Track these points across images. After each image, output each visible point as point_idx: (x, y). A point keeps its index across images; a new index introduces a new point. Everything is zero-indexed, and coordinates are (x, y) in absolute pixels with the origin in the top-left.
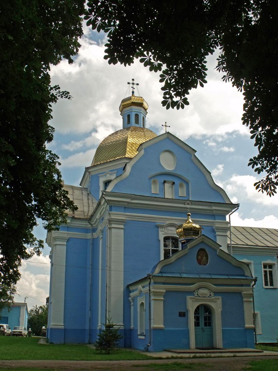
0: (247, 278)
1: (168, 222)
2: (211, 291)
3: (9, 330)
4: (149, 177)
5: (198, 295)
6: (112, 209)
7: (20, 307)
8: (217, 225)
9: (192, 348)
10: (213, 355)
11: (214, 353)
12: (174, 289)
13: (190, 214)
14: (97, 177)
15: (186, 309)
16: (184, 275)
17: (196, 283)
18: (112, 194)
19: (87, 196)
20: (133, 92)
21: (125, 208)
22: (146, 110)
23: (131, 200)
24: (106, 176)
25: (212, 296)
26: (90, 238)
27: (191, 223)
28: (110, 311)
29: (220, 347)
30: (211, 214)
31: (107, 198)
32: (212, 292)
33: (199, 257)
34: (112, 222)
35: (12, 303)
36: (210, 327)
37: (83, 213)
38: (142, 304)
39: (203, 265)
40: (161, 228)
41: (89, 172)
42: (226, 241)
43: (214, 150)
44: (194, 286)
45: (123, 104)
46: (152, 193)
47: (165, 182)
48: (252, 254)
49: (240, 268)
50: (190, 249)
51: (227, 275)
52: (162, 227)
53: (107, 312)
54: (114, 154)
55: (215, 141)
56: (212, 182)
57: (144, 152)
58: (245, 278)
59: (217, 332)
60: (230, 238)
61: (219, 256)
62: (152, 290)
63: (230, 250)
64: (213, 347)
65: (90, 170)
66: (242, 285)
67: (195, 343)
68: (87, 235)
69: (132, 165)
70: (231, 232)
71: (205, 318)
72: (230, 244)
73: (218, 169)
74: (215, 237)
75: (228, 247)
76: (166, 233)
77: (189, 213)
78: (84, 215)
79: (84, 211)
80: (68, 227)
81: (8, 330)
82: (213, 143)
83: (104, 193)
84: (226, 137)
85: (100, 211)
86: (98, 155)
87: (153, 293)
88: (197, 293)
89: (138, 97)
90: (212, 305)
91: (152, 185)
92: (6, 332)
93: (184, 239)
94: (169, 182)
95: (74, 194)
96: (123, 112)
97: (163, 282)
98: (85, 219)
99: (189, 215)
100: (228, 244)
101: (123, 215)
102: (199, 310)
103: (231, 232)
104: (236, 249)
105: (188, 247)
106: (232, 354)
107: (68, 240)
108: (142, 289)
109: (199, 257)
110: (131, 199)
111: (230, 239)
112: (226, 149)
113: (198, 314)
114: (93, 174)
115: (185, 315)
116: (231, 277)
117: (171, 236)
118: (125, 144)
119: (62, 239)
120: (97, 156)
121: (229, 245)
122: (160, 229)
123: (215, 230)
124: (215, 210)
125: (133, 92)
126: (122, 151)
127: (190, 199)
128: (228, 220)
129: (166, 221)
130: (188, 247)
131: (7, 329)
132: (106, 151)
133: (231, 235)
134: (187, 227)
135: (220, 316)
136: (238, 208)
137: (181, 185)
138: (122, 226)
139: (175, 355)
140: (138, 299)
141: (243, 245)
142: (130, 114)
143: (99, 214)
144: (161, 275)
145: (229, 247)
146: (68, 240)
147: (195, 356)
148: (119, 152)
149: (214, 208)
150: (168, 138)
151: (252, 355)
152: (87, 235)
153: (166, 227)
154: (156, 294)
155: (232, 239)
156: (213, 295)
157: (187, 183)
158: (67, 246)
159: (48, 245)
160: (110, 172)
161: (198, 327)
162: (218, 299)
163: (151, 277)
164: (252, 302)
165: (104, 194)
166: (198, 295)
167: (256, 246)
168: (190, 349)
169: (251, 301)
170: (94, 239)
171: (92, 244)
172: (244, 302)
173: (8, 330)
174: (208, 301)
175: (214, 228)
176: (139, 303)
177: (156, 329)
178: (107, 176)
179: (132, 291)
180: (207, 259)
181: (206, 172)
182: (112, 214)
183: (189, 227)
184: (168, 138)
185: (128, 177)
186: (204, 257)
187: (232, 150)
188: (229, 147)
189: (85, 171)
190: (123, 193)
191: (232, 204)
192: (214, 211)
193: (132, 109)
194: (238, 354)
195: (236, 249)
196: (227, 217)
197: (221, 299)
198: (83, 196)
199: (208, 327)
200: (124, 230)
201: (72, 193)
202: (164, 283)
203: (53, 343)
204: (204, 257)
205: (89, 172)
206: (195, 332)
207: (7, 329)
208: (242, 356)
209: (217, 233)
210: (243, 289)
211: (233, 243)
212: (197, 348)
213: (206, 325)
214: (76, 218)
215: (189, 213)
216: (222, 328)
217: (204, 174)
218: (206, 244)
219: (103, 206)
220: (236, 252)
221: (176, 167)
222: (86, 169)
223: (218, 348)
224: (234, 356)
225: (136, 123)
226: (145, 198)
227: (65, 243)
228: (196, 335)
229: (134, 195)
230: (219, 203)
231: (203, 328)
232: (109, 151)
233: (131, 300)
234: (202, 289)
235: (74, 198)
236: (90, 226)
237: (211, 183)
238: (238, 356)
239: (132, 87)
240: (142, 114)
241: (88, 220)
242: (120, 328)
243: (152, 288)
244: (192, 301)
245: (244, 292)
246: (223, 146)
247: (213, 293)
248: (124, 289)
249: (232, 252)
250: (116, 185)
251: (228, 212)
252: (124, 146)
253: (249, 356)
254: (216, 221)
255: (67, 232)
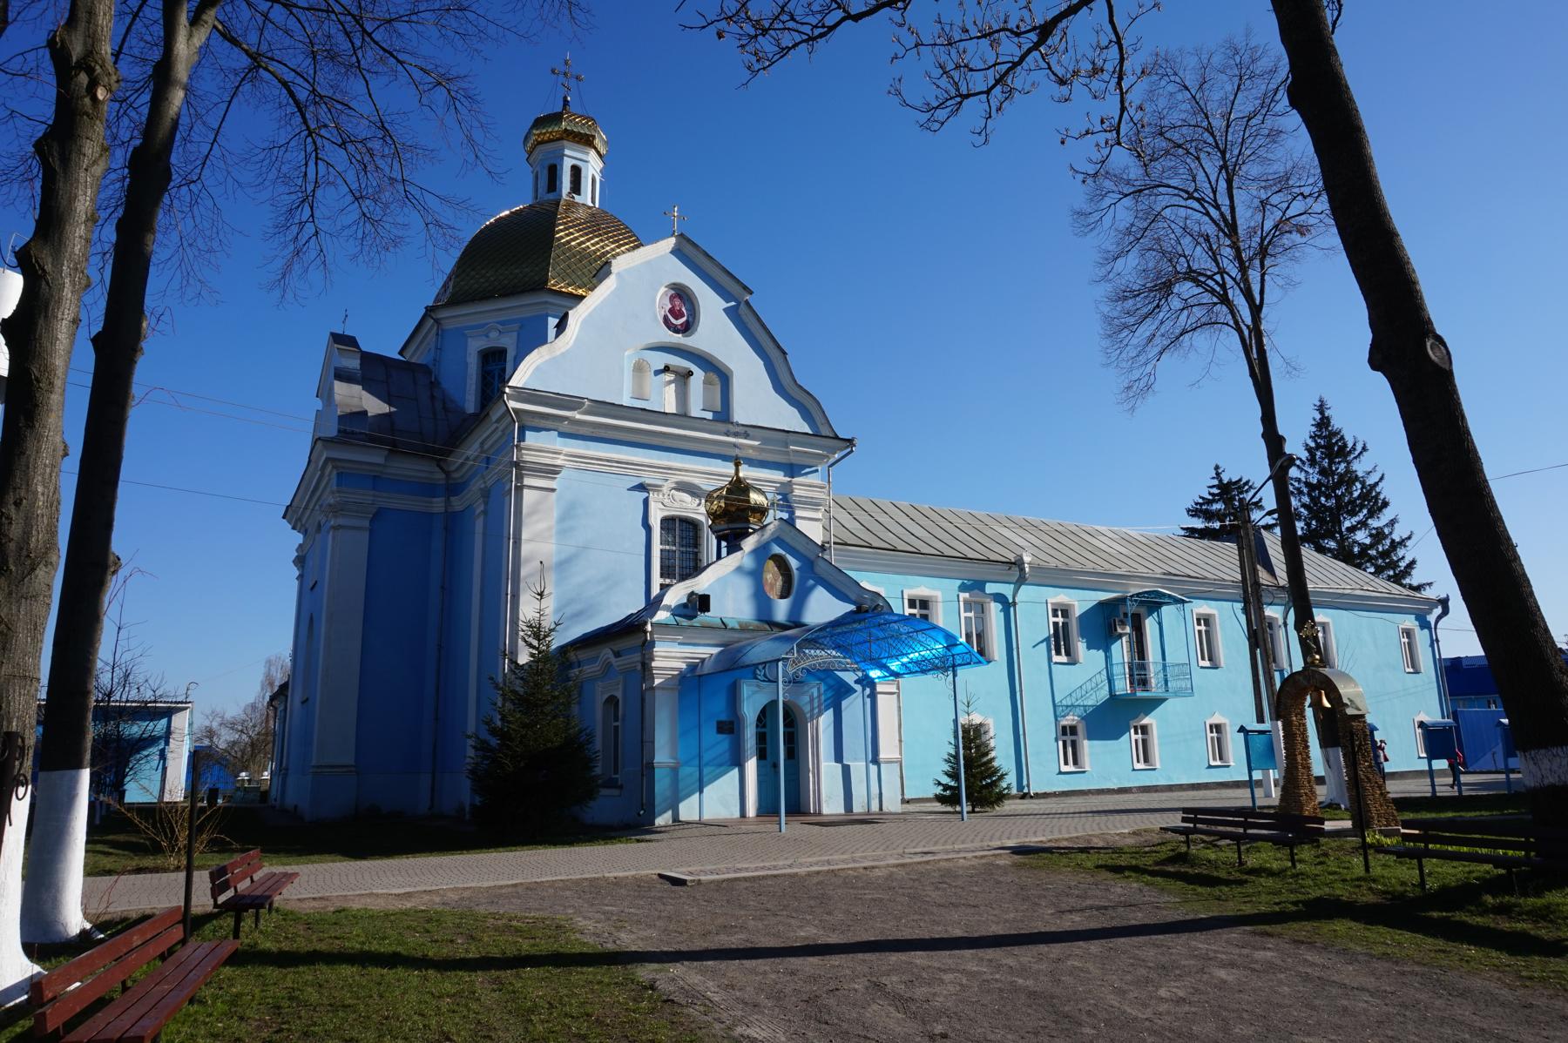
5: (765, 675)
38: (612, 701)
41: (437, 321)
80: (375, 476)
85: (485, 435)
93: (725, 526)
108: (613, 659)
113: (764, 726)
143: (477, 445)
152: (431, 503)
159: (290, 526)
160: (500, 327)
166: (765, 675)
179: (576, 664)
205: (437, 321)
219: (495, 425)
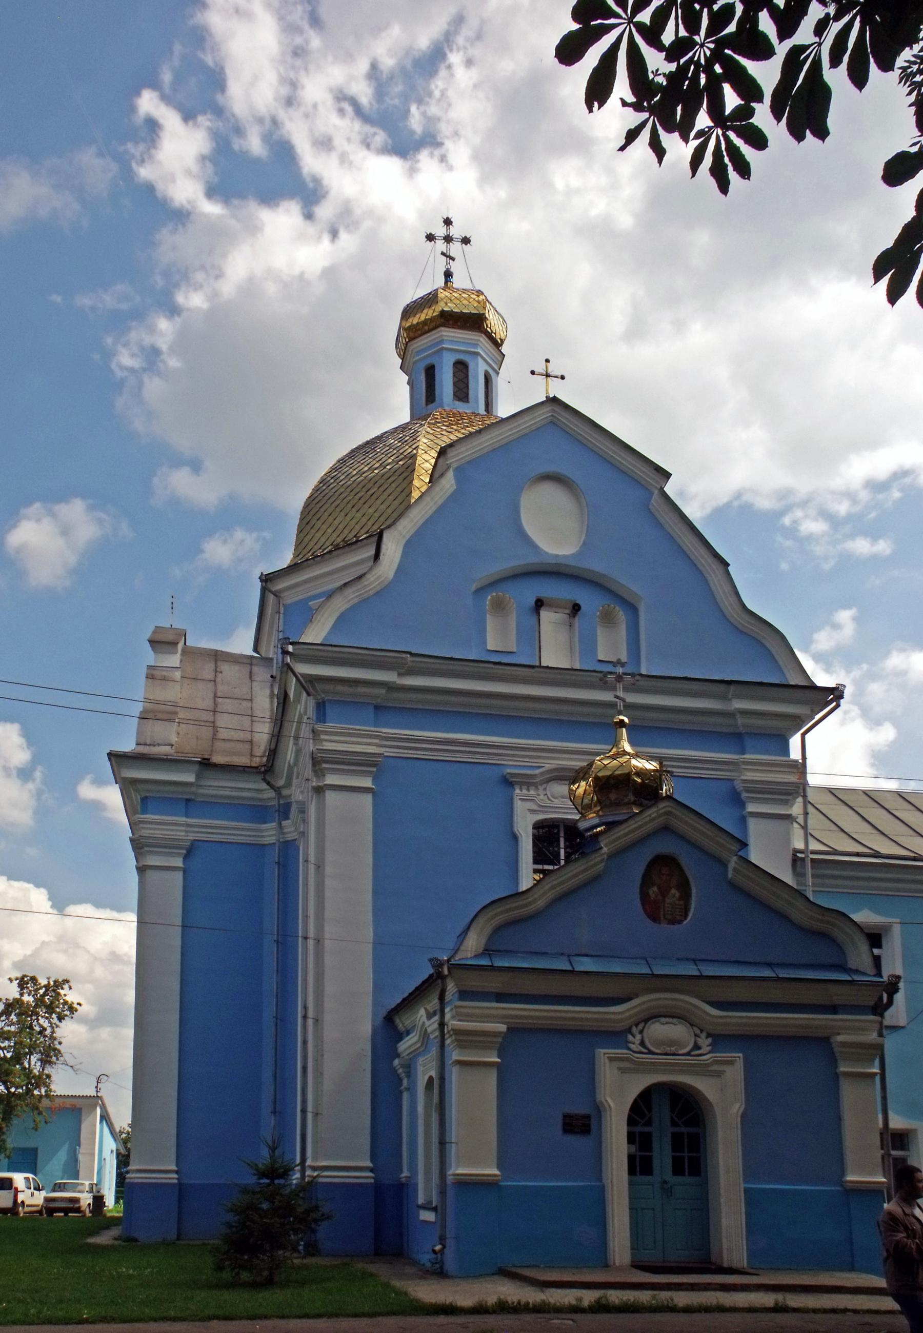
0: (856, 978)
1: (551, 764)
2: (702, 1031)
3: (36, 1192)
4: (474, 587)
5: (642, 1044)
6: (327, 708)
7: (81, 1109)
8: (749, 776)
9: (617, 1263)
10: (682, 1299)
11: (699, 1290)
12: (532, 1017)
13: (626, 720)
15: (595, 1101)
16: (586, 965)
17: (637, 996)
18: (317, 654)
19: (268, 684)
20: (448, 275)
21: (377, 708)
22: (497, 344)
23: (400, 675)
25: (705, 1049)
26: (272, 840)
27: (629, 754)
28: (321, 1114)
29: (736, 1264)
30: (724, 730)
31: (303, 669)
32: (703, 1035)
33: (653, 891)
34: (324, 765)
35: (47, 1096)
36: (692, 1180)
37: (247, 746)
39: (669, 924)
40: (525, 787)
41: (276, 594)
42: (788, 839)
43: (818, 550)
44: (628, 1010)
45: (408, 325)
46: (489, 648)
47: (539, 604)
48: (905, 890)
49: (823, 936)
50: (612, 856)
51: (769, 965)
52: (528, 782)
53: (310, 1116)
54: (364, 520)
55: (825, 515)
56: (733, 599)
57: (453, 482)
58: (849, 978)
59: (722, 1200)
60: (805, 827)
61: (734, 886)
62: (452, 1022)
63: (803, 875)
64: (710, 1263)
65: (280, 585)
66: (834, 1009)
67: (628, 1244)
68: (262, 831)
69: (408, 537)
70: (806, 802)
71: (677, 1142)
72: (801, 852)
73: (836, 627)
74: (743, 821)
75: (797, 860)
76: (543, 808)
77: (621, 717)
78: (252, 755)
79: (251, 742)
80: (188, 800)
81: (32, 1195)
82: (817, 520)
83: (290, 648)
84: (864, 495)
86: (308, 527)
87: (454, 1037)
88: (639, 1037)
89: (464, 291)
90: (704, 1086)
91: (488, 616)
92: (23, 1202)
94: (554, 605)
95: (218, 680)
96: (408, 356)
97: (497, 991)
98: (250, 770)
99: (621, 724)
100: (796, 851)
101: (371, 737)
102: (650, 1110)
103: (806, 802)
104: (827, 872)
105: (605, 849)
106: (768, 1299)
107: (190, 852)
109: (651, 893)
110: (402, 671)
111: (802, 832)
112: (862, 546)
113: (649, 1123)
114: (289, 601)
115: (589, 1126)
116: (783, 974)
117: (563, 821)
118: (405, 475)
120: (305, 532)
121: (798, 855)
122: (517, 791)
123: (744, 795)
124: (745, 713)
125: (448, 275)
126: (397, 502)
127: (644, 672)
128: (795, 753)
129: (539, 757)
130: (602, 848)
131: (29, 1192)
132: (338, 510)
133: (806, 814)
134: (609, 773)
135: (736, 1135)
136: (838, 706)
137: (607, 618)
138: (367, 782)
139: (532, 1296)
140: (419, 1067)
141: (858, 855)
144: (490, 964)
145: (799, 863)
146: (190, 852)
147: (603, 1301)
148: (383, 507)
149: (739, 705)
150: (554, 424)
151: (858, 1308)
152: (262, 831)
153: (542, 783)
154: (466, 1039)
155: (810, 831)
156: (710, 1048)
157: (632, 608)
161: (646, 1179)
162: (731, 1063)
163: (446, 972)
164: (878, 1079)
165: (288, 653)
166: (642, 1044)
167: (914, 859)
168: (606, 1266)
169: (874, 1075)
170: (286, 842)
171: (278, 863)
172: (841, 1079)
173: (32, 1195)
174: (682, 1072)
175: (739, 786)
176: (424, 1078)
177: (467, 1185)
179: (405, 1034)
180: (686, 896)
181: (710, 560)
182: (326, 733)
183: (617, 773)
184: (553, 423)
185: (390, 583)
186: (673, 891)
187: (883, 547)
188: (875, 538)
189: (264, 591)
190: (366, 649)
191: (813, 687)
192: (738, 716)
193: (442, 342)
194: (794, 1300)
195: (827, 872)
196: (795, 742)
197: (740, 1064)
198: (255, 684)
199: (686, 1179)
200: (373, 795)
201: (211, 677)
202: (500, 997)
203: (136, 1240)
204: (673, 891)
205: (276, 594)
206: (630, 1198)
207: (29, 1192)
208: (815, 1311)
209: (751, 808)
210: (840, 1023)
211: (814, 846)
212: (637, 1265)
213: (678, 1170)
214: (215, 765)
215: (621, 717)
216: (745, 1181)
217: (701, 568)
218: (682, 837)
220: (827, 881)
221: (584, 543)
222: (261, 581)
223: (725, 1265)
224: (778, 1309)
225: (460, 400)
226: (458, 667)
227: (179, 862)
228: (634, 1210)
229: (410, 653)
230: (761, 684)
231: (665, 1182)
232: (350, 506)
233: (403, 1075)
234: (663, 1020)
235: (219, 694)
236: (271, 794)
237: (727, 603)
238: (795, 1310)
239: (443, 254)
240: (480, 360)
241: (260, 773)
242: (321, 1180)
243: (453, 1017)
244: (619, 1069)
245: (840, 1038)
246: (853, 536)
247: (710, 1040)
248: (373, 1026)
249: (810, 881)
250: (343, 618)
251: (797, 722)
252: (404, 485)
253: (845, 1311)
254: (747, 756)
255: (184, 819)
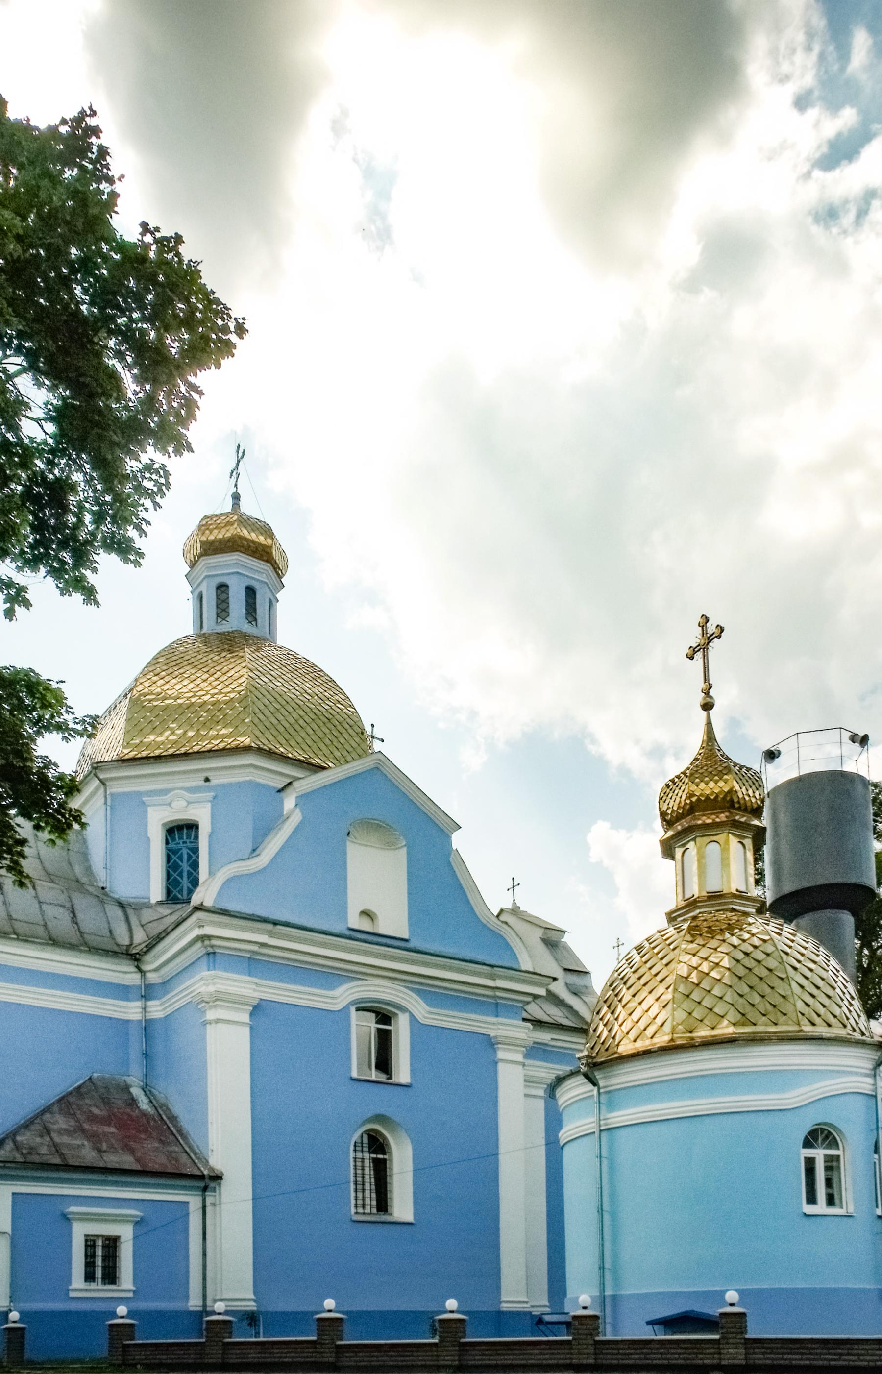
14: (139, 802)
20: (236, 497)
24: (170, 804)
119: (235, 1001)
125: (236, 497)
142: (229, 583)
146: (258, 1009)
158: (251, 1028)
160: (187, 795)
178: (173, 805)
227: (246, 1018)
